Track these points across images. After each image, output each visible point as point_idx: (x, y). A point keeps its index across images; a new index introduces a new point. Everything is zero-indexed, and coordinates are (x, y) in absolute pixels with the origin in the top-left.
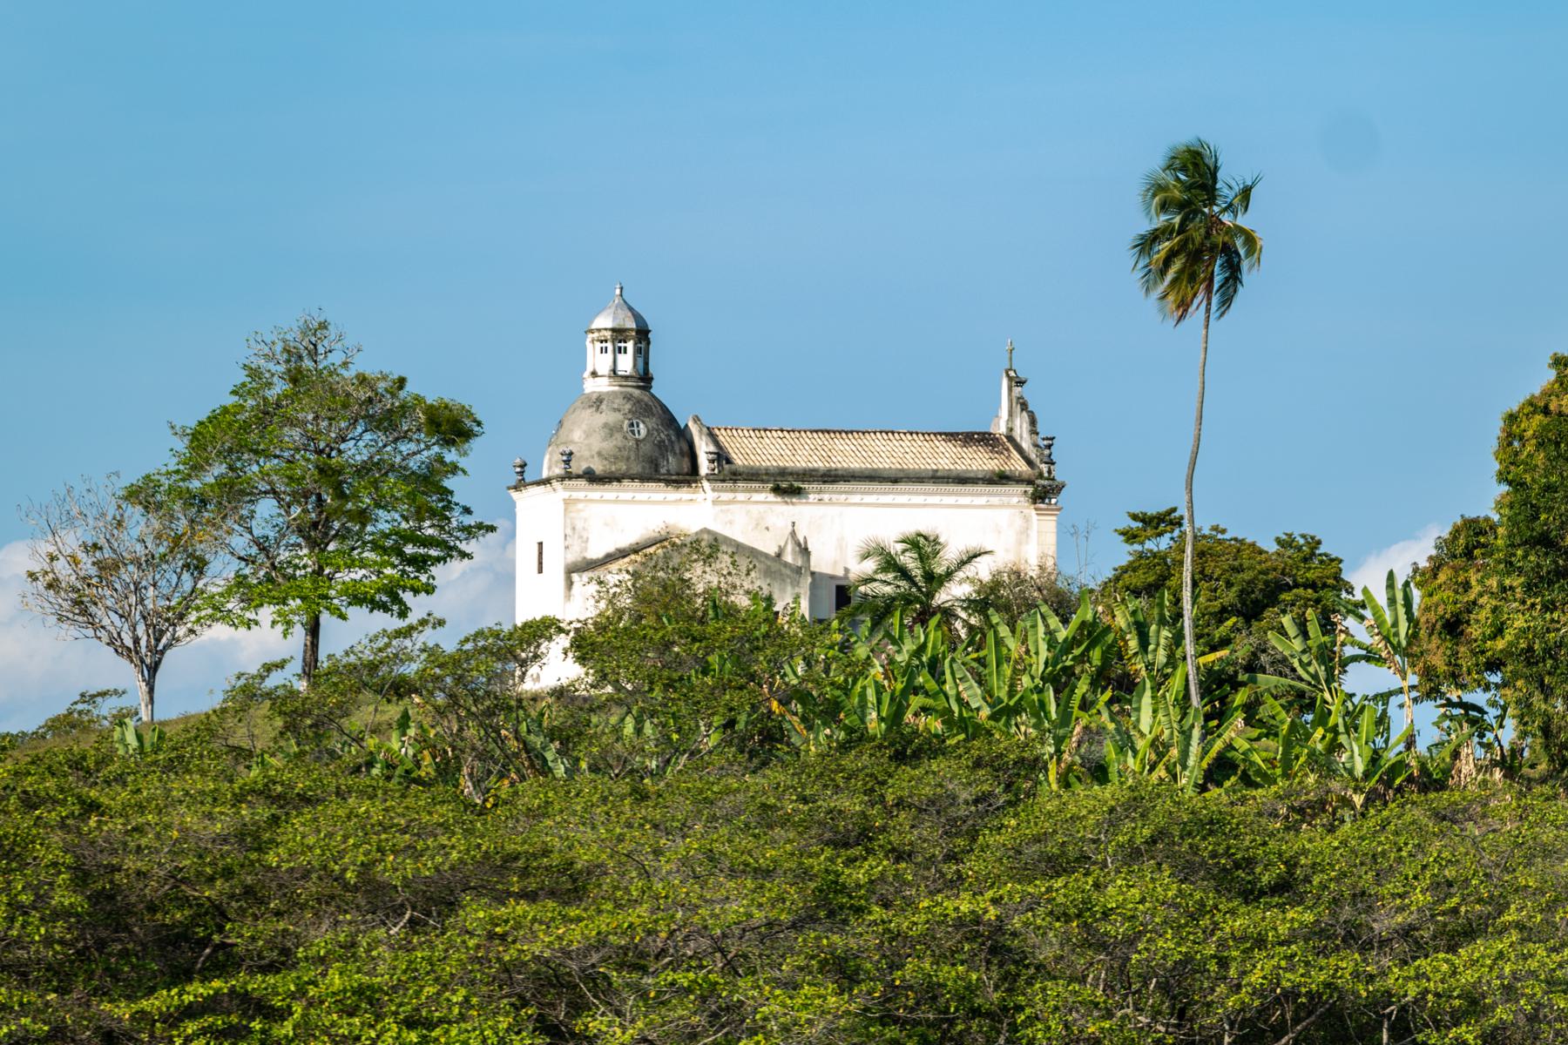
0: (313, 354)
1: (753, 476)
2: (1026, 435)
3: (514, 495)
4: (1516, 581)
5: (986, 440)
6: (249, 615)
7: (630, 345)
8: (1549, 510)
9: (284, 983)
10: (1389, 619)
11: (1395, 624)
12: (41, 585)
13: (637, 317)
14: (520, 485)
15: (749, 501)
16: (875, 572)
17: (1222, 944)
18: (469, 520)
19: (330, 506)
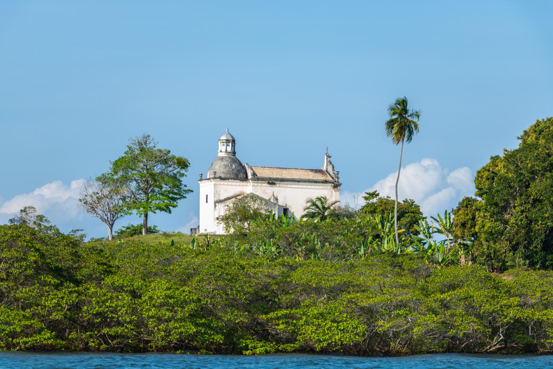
0: (146, 143)
1: (262, 179)
2: (331, 171)
3: (199, 182)
6: (130, 211)
7: (230, 144)
8: (497, 196)
9: (299, 311)
10: (444, 222)
11: (446, 224)
12: (83, 202)
13: (232, 137)
14: (201, 180)
15: (261, 186)
17: (501, 307)
18: (185, 188)
19: (151, 181)
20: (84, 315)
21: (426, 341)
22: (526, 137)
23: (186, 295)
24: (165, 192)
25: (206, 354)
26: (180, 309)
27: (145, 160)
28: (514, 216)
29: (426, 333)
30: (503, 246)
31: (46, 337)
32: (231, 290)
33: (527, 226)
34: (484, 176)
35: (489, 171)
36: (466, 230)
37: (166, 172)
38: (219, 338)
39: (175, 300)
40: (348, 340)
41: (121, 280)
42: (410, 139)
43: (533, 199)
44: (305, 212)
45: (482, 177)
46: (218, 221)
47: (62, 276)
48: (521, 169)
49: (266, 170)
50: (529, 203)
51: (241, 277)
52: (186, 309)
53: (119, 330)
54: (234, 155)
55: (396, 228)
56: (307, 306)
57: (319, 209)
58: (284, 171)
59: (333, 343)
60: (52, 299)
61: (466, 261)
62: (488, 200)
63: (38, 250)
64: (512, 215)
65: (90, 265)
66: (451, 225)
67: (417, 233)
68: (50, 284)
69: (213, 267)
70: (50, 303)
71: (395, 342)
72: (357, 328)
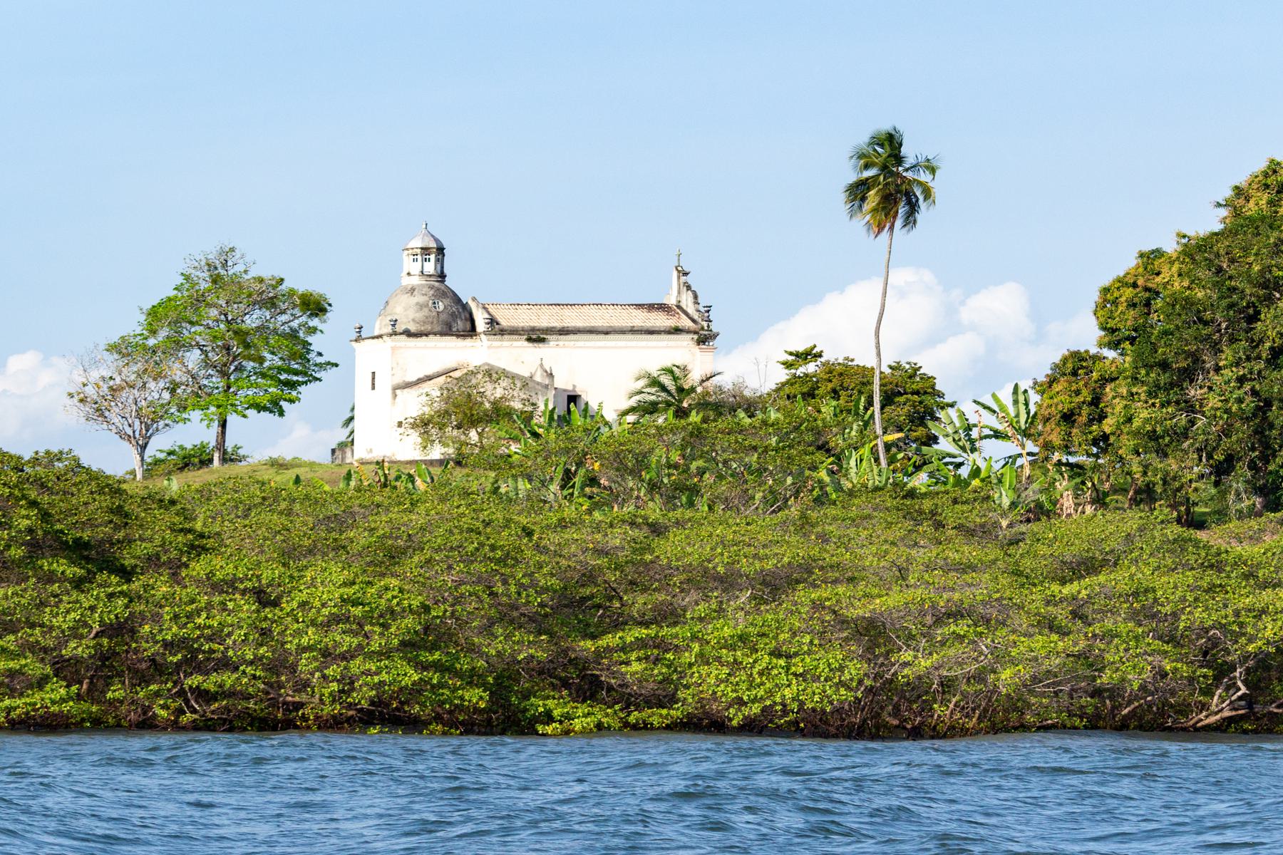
1: (514, 332)
4: (1141, 390)
5: (662, 307)
6: (185, 416)
7: (432, 257)
11: (1017, 416)
13: (437, 240)
16: (647, 386)
17: (1237, 613)
18: (319, 360)
19: (236, 350)
20: (145, 645)
21: (1033, 700)
22: (1242, 201)
23: (394, 597)
24: (270, 369)
25: (444, 733)
26: (377, 629)
27: (222, 302)
28: (1218, 392)
29: (1035, 679)
30: (1189, 468)
31: (55, 696)
32: (505, 582)
33: (1255, 415)
34: (1123, 299)
35: (1135, 285)
36: (1075, 431)
37: (271, 326)
38: (476, 697)
39: (367, 608)
40: (817, 698)
41: (231, 566)
42: (910, 220)
43: (1272, 348)
44: (633, 402)
45: (1115, 302)
46: (401, 430)
47: (88, 559)
48: (1230, 278)
49: (522, 309)
50: (1259, 357)
51: (528, 553)
52: (392, 630)
53: (228, 679)
54: (443, 282)
55: (879, 431)
56: (701, 619)
57: (670, 397)
58: (567, 311)
59: (779, 708)
60: (68, 612)
61: (1077, 505)
62: (1138, 356)
63: (33, 504)
64: (1210, 388)
65: (158, 532)
66: (1032, 420)
67: (933, 439)
68: (63, 579)
69: (456, 531)
70: (63, 621)
71: (944, 702)
72: (841, 669)
